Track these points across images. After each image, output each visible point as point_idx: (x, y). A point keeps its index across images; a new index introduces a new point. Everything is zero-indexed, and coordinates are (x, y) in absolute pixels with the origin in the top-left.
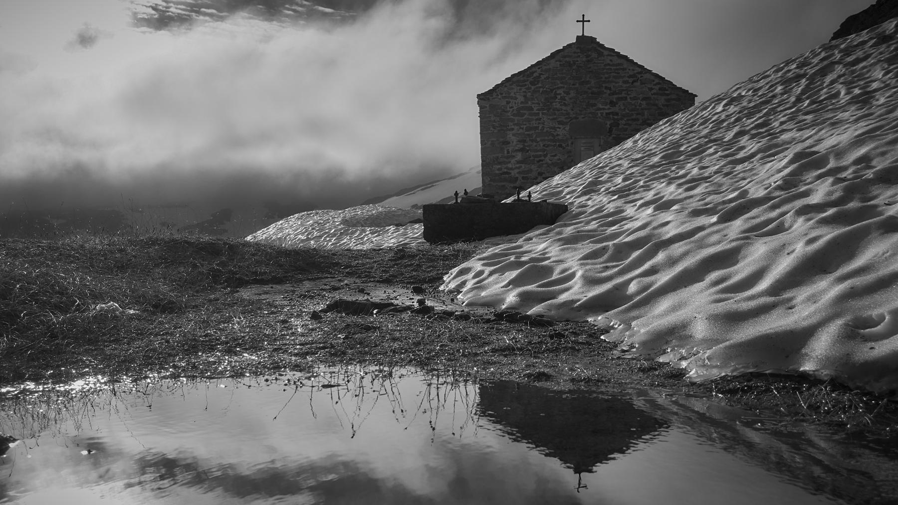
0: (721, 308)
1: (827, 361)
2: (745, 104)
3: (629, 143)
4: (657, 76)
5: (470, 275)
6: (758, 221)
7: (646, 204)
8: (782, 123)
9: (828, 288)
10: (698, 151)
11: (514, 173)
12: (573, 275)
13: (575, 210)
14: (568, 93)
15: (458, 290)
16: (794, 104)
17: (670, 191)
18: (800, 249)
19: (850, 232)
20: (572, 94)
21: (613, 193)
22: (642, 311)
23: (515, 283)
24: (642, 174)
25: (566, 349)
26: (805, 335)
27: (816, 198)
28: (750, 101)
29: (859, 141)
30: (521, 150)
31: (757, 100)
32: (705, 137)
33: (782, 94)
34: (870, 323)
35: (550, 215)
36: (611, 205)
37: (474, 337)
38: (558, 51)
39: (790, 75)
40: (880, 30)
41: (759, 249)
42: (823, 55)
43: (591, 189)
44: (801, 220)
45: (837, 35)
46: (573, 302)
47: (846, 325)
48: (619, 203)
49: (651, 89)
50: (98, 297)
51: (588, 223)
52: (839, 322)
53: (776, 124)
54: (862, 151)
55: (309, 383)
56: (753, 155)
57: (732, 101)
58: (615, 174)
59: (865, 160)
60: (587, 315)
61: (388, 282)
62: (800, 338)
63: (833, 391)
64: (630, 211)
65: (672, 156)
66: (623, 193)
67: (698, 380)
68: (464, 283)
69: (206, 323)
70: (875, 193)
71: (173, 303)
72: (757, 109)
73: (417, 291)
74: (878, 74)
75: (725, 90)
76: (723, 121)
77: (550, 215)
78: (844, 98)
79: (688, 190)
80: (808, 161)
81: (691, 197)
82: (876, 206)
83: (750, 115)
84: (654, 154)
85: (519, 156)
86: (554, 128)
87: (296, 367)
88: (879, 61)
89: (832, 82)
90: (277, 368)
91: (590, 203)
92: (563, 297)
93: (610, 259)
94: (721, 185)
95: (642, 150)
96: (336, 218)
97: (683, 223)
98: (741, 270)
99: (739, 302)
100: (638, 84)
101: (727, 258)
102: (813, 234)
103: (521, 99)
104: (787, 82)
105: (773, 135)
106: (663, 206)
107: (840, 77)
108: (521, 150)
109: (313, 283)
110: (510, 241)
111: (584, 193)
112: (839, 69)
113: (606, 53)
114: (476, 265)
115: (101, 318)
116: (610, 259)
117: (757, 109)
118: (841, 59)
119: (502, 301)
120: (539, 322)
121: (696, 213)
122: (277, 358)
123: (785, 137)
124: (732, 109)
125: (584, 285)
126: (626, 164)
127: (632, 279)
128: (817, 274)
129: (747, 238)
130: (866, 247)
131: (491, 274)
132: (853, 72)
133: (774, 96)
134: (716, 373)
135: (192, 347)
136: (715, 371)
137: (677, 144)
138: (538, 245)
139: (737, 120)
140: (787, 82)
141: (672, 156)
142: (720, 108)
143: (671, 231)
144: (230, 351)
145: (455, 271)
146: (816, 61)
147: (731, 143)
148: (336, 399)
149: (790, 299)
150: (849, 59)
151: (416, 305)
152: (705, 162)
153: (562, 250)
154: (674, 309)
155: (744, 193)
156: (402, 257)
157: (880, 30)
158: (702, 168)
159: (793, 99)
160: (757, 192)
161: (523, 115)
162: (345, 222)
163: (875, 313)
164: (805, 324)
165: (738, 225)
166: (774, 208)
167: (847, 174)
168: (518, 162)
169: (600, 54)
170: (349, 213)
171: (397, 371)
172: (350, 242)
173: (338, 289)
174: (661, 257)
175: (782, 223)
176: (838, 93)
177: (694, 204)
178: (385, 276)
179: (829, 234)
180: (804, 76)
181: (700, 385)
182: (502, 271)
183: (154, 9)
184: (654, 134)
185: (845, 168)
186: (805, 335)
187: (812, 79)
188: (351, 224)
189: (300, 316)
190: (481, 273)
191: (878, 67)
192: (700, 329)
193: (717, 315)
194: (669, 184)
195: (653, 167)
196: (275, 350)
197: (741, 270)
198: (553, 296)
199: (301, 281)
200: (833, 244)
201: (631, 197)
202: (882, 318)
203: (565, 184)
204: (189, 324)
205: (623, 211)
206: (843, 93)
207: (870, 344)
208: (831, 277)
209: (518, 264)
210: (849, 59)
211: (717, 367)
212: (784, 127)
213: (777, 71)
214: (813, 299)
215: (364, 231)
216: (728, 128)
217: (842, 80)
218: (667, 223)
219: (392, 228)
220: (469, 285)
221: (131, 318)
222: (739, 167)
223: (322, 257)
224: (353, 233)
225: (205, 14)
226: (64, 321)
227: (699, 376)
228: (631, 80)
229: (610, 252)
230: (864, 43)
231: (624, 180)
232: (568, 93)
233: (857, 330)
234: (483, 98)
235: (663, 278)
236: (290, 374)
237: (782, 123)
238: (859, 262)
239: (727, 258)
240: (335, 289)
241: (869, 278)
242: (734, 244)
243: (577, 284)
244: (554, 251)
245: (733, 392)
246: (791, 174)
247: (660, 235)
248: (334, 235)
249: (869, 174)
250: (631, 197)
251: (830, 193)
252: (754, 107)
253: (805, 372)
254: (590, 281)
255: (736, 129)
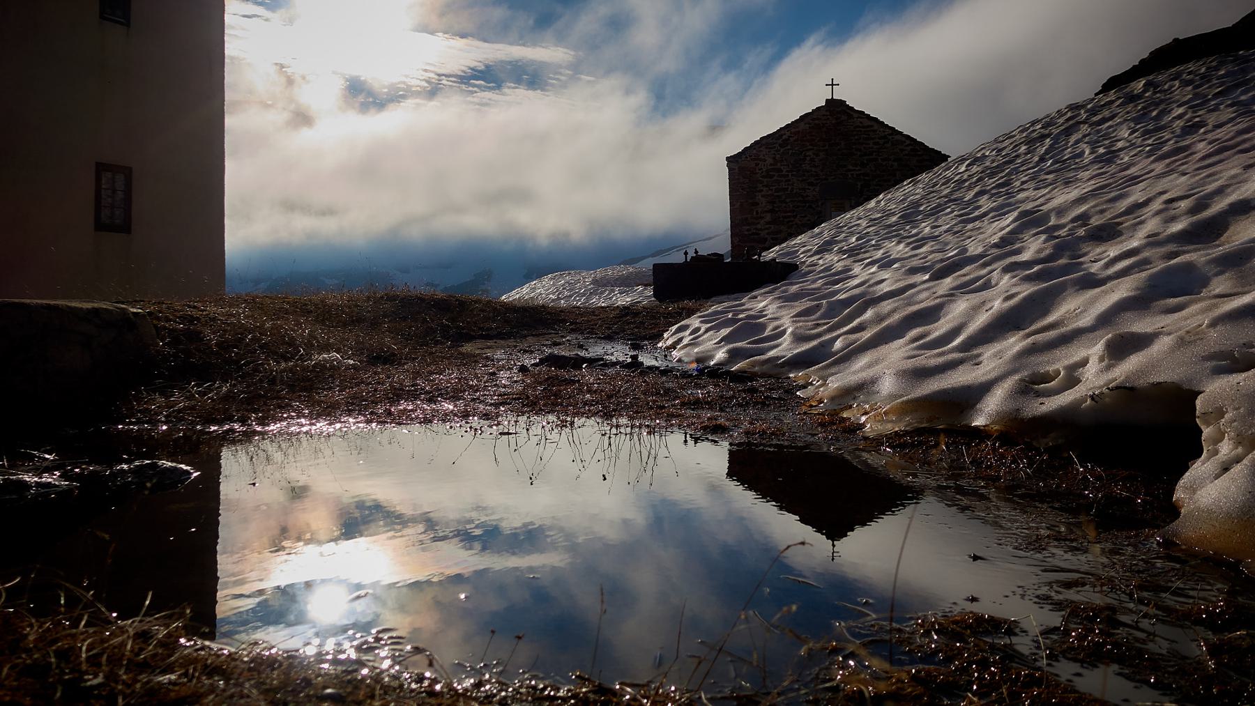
0: (910, 364)
1: (1001, 417)
2: (988, 164)
3: (872, 203)
4: (908, 137)
5: (688, 332)
6: (968, 278)
7: (872, 263)
8: (1023, 183)
9: (1014, 343)
10: (936, 212)
11: (763, 234)
12: (784, 332)
13: (804, 269)
14: (817, 155)
15: (673, 346)
16: (1038, 164)
17: (898, 249)
18: (998, 305)
19: (1047, 288)
20: (822, 155)
21: (844, 252)
22: (842, 366)
23: (726, 339)
24: (877, 233)
25: (756, 403)
26: (985, 388)
27: (1025, 256)
28: (993, 161)
29: (1080, 200)
30: (771, 211)
31: (1001, 160)
32: (946, 196)
33: (1026, 154)
34: (1047, 378)
35: (783, 272)
36: (840, 264)
37: (667, 391)
38: (807, 115)
39: (1034, 135)
40: (1128, 90)
41: (960, 306)
42: (1069, 114)
43: (824, 249)
44: (1007, 277)
45: (1096, 94)
46: (778, 358)
47: (1021, 380)
48: (848, 262)
49: (902, 150)
50: (326, 348)
51: (814, 281)
52: (1017, 377)
53: (1018, 183)
54: (1083, 208)
55: (490, 430)
56: (985, 215)
57: (976, 161)
58: (852, 234)
59: (1083, 218)
60: (790, 371)
61: (609, 338)
62: (972, 396)
63: (1000, 447)
64: (857, 269)
65: (910, 217)
66: (853, 252)
67: (871, 435)
68: (680, 340)
69: (417, 374)
70: (1085, 250)
71: (394, 355)
72: (1000, 168)
73: (635, 347)
74: (1124, 133)
75: (969, 151)
76: (966, 181)
77: (783, 272)
78: (1088, 156)
79: (913, 249)
80: (1032, 220)
81: (916, 255)
82: (1082, 263)
83: (991, 176)
84: (893, 214)
85: (768, 217)
86: (804, 189)
87: (486, 416)
88: (1126, 120)
89: (1077, 142)
90: (465, 415)
91: (821, 262)
92: (772, 353)
93: (823, 317)
94: (947, 244)
95: (884, 211)
96: (587, 278)
97: (897, 281)
98: (939, 329)
99: (931, 359)
100: (889, 145)
101: (929, 315)
102: (1014, 290)
103: (769, 161)
104: (1031, 142)
105: (1009, 195)
106: (886, 263)
107: (1085, 136)
108: (771, 211)
109: (535, 339)
110: (736, 300)
111: (817, 253)
112: (1085, 129)
113: (855, 115)
114: (694, 322)
115: (321, 366)
116: (823, 317)
117: (1000, 168)
118: (1087, 119)
119: (712, 357)
120: (740, 377)
121: (913, 271)
122: (476, 406)
123: (1021, 196)
124: (975, 169)
125: (793, 342)
126: (864, 223)
127: (838, 337)
128: (1010, 330)
129: (952, 295)
130: (1060, 304)
131: (707, 331)
132: (1099, 131)
133: (1018, 156)
134: (890, 428)
135: (398, 394)
136: (889, 426)
137: (917, 204)
138: (763, 303)
139: (978, 180)
140: (1031, 142)
141: (910, 217)
142: (963, 168)
143: (885, 288)
144: (431, 400)
145: (674, 328)
146: (1061, 121)
147: (969, 203)
148: (513, 446)
149: (979, 355)
150: (1095, 119)
151: (629, 360)
152: (940, 222)
153: (780, 307)
154: (870, 365)
155: (966, 250)
156: (626, 315)
157: (1128, 90)
158: (933, 227)
159: (1036, 159)
160: (974, 249)
161: (772, 177)
162: (595, 282)
163: (1051, 369)
164: (984, 379)
165: (948, 282)
166: (985, 265)
167: (1063, 232)
168: (767, 223)
169: (850, 116)
170: (599, 273)
171: (578, 421)
172: (599, 302)
173: (559, 344)
174: (869, 314)
175: (989, 280)
176: (1083, 152)
177: (915, 263)
178: (608, 332)
179: (1027, 290)
180: (1048, 136)
181: (873, 439)
182: (717, 328)
183: (428, 82)
184: (898, 194)
185: (1063, 226)
186: (985, 388)
187: (1056, 140)
188: (601, 284)
189: (509, 366)
190: (698, 329)
191: (1124, 126)
192: (887, 385)
193: (904, 371)
194: (899, 243)
195: (890, 226)
196: (473, 400)
197: (939, 329)
198: (762, 352)
199: (526, 337)
200: (1030, 300)
201: (860, 257)
202: (1058, 373)
203: (802, 246)
204: (400, 376)
205: (850, 270)
206: (1087, 152)
207: (1041, 400)
208: (1022, 333)
209: (734, 321)
210: (1095, 119)
211: (892, 421)
212: (1025, 186)
213: (1022, 131)
214: (998, 355)
215: (613, 291)
216: (970, 188)
217: (1087, 139)
218: (883, 281)
219: (640, 288)
220: (685, 341)
221: (348, 367)
222: (970, 226)
223: (549, 313)
224: (602, 293)
225: (475, 86)
226: (284, 370)
227: (873, 430)
228: (881, 142)
229: (822, 310)
230: (1112, 102)
231: (858, 239)
232: (817, 155)
233: (1032, 386)
234: (730, 160)
235: (866, 335)
236: (475, 421)
237: (1023, 183)
238: (1051, 318)
239: (929, 315)
240: (555, 344)
241: (1052, 334)
242: (937, 301)
243: (786, 340)
244: (772, 310)
245: (903, 446)
246: (1010, 233)
247: (874, 292)
248: (584, 294)
249: (1081, 232)
250: (860, 257)
251: (1040, 251)
252: (997, 167)
253: (976, 427)
254: (799, 338)
255: (977, 189)
